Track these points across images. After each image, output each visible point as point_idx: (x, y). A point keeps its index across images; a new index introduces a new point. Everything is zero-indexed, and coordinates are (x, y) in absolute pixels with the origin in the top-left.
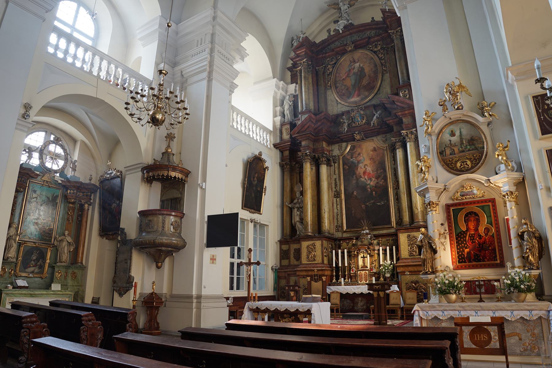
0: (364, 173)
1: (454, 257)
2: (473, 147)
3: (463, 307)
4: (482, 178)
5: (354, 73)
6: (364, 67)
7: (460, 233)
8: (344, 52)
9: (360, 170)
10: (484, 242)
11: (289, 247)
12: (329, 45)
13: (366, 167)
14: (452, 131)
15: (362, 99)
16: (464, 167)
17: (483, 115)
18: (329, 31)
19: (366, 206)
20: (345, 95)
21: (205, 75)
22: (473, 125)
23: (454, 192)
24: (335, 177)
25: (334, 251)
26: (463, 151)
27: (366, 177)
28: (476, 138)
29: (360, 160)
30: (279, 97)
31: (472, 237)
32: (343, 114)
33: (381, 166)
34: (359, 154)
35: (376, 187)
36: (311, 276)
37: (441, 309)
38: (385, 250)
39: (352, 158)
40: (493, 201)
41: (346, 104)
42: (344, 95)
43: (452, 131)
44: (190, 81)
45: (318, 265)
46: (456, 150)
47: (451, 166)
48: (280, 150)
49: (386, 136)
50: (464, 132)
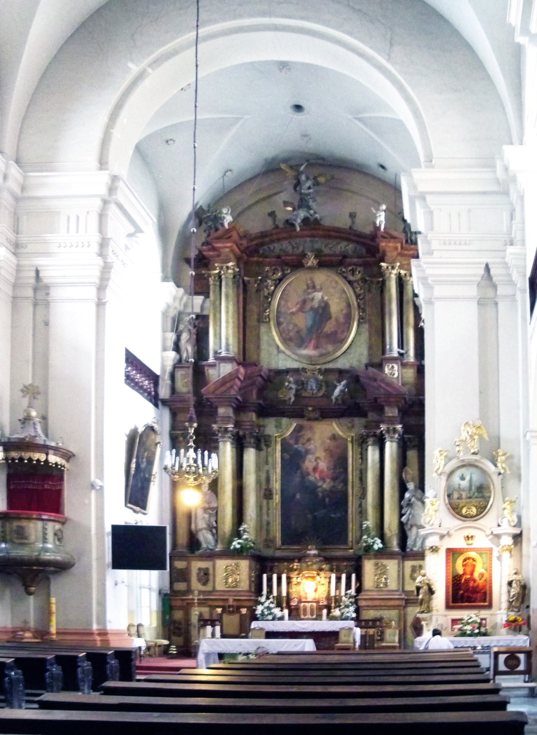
0: (315, 469)
2: (481, 495)
5: (312, 309)
6: (330, 303)
8: (297, 264)
9: (309, 464)
11: (189, 564)
12: (272, 241)
13: (317, 461)
14: (463, 475)
17: (496, 465)
19: (315, 517)
20: (294, 340)
21: (92, 293)
22: (484, 472)
25: (265, 576)
26: (470, 498)
27: (317, 475)
29: (310, 450)
30: (173, 313)
32: (287, 371)
34: (309, 440)
36: (223, 607)
39: (296, 443)
41: (293, 356)
42: (291, 339)
43: (463, 475)
45: (241, 594)
46: (464, 495)
47: (455, 509)
48: (171, 410)
49: (353, 420)
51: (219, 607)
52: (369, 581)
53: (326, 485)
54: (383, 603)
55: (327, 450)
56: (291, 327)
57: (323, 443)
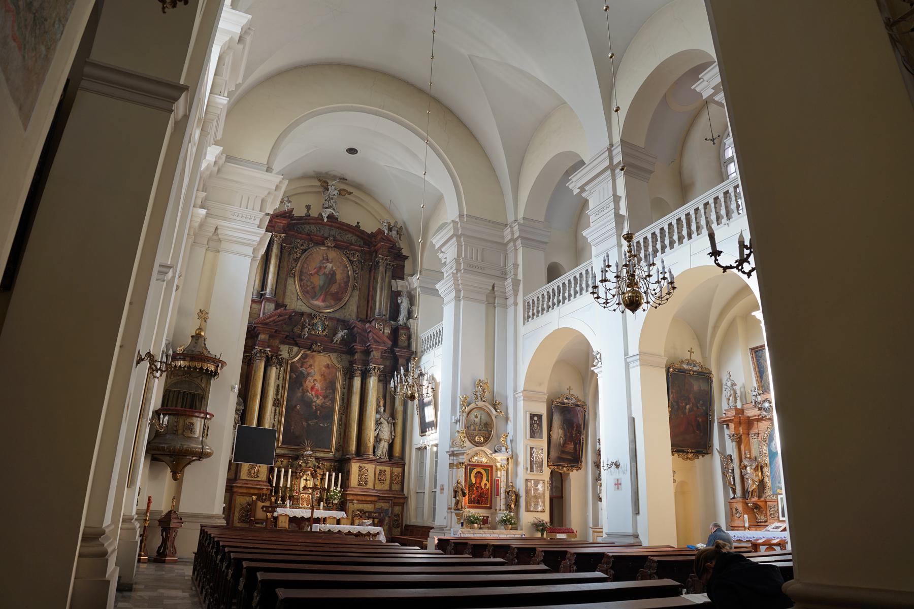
0: (312, 388)
4: (489, 452)
5: (324, 274)
9: (308, 384)
12: (304, 224)
15: (327, 307)
18: (308, 207)
19: (308, 425)
20: (309, 292)
22: (489, 415)
24: (278, 382)
31: (477, 488)
32: (302, 314)
33: (331, 386)
34: (310, 366)
35: (322, 406)
38: (330, 475)
40: (491, 467)
42: (308, 292)
44: (224, 245)
50: (483, 417)
51: (255, 494)
52: (354, 480)
53: (319, 401)
54: (363, 498)
55: (322, 375)
56: (309, 283)
57: (320, 369)
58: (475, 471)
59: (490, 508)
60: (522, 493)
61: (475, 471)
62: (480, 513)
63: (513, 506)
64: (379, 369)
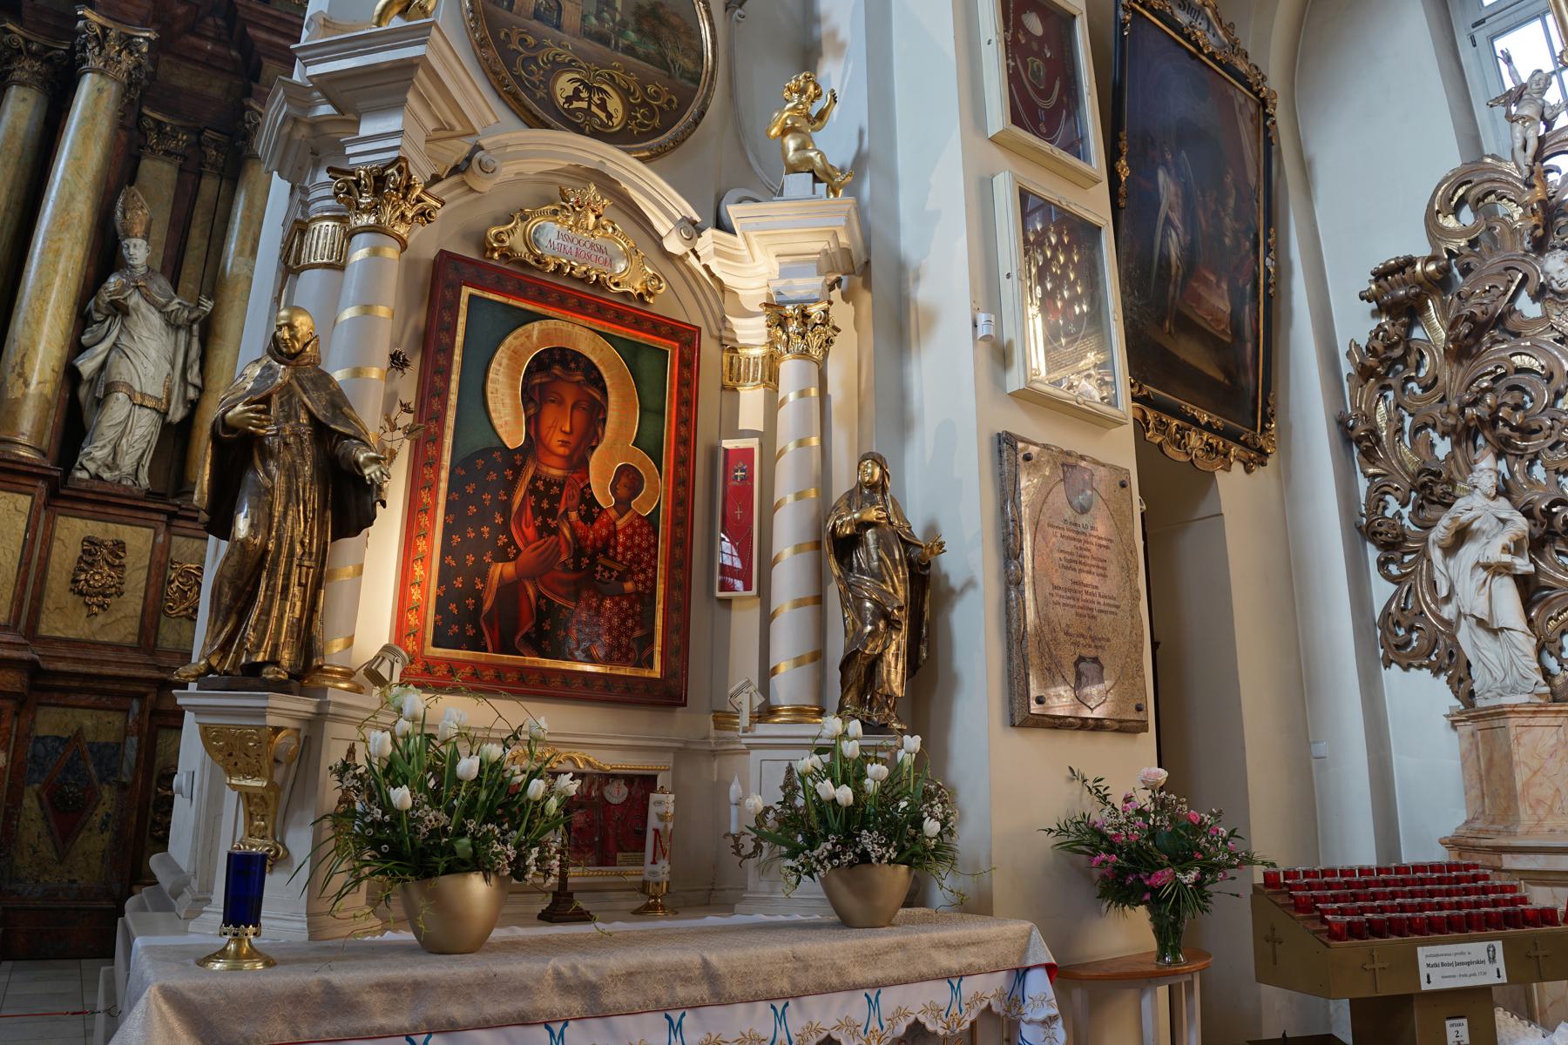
1: (416, 594)
2: (652, 49)
3: (590, 990)
7: (486, 452)
10: (607, 545)
16: (588, 112)
23: (498, 206)
26: (603, 39)
28: (674, 20)
31: (546, 496)
37: (403, 1021)
40: (686, 336)
58: (530, 339)
59: (668, 695)
60: (968, 557)
61: (530, 339)
62: (558, 739)
63: (894, 675)
64: (128, 43)
